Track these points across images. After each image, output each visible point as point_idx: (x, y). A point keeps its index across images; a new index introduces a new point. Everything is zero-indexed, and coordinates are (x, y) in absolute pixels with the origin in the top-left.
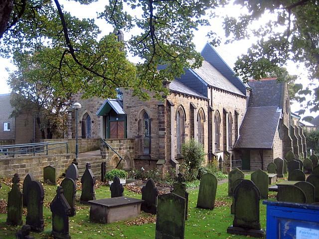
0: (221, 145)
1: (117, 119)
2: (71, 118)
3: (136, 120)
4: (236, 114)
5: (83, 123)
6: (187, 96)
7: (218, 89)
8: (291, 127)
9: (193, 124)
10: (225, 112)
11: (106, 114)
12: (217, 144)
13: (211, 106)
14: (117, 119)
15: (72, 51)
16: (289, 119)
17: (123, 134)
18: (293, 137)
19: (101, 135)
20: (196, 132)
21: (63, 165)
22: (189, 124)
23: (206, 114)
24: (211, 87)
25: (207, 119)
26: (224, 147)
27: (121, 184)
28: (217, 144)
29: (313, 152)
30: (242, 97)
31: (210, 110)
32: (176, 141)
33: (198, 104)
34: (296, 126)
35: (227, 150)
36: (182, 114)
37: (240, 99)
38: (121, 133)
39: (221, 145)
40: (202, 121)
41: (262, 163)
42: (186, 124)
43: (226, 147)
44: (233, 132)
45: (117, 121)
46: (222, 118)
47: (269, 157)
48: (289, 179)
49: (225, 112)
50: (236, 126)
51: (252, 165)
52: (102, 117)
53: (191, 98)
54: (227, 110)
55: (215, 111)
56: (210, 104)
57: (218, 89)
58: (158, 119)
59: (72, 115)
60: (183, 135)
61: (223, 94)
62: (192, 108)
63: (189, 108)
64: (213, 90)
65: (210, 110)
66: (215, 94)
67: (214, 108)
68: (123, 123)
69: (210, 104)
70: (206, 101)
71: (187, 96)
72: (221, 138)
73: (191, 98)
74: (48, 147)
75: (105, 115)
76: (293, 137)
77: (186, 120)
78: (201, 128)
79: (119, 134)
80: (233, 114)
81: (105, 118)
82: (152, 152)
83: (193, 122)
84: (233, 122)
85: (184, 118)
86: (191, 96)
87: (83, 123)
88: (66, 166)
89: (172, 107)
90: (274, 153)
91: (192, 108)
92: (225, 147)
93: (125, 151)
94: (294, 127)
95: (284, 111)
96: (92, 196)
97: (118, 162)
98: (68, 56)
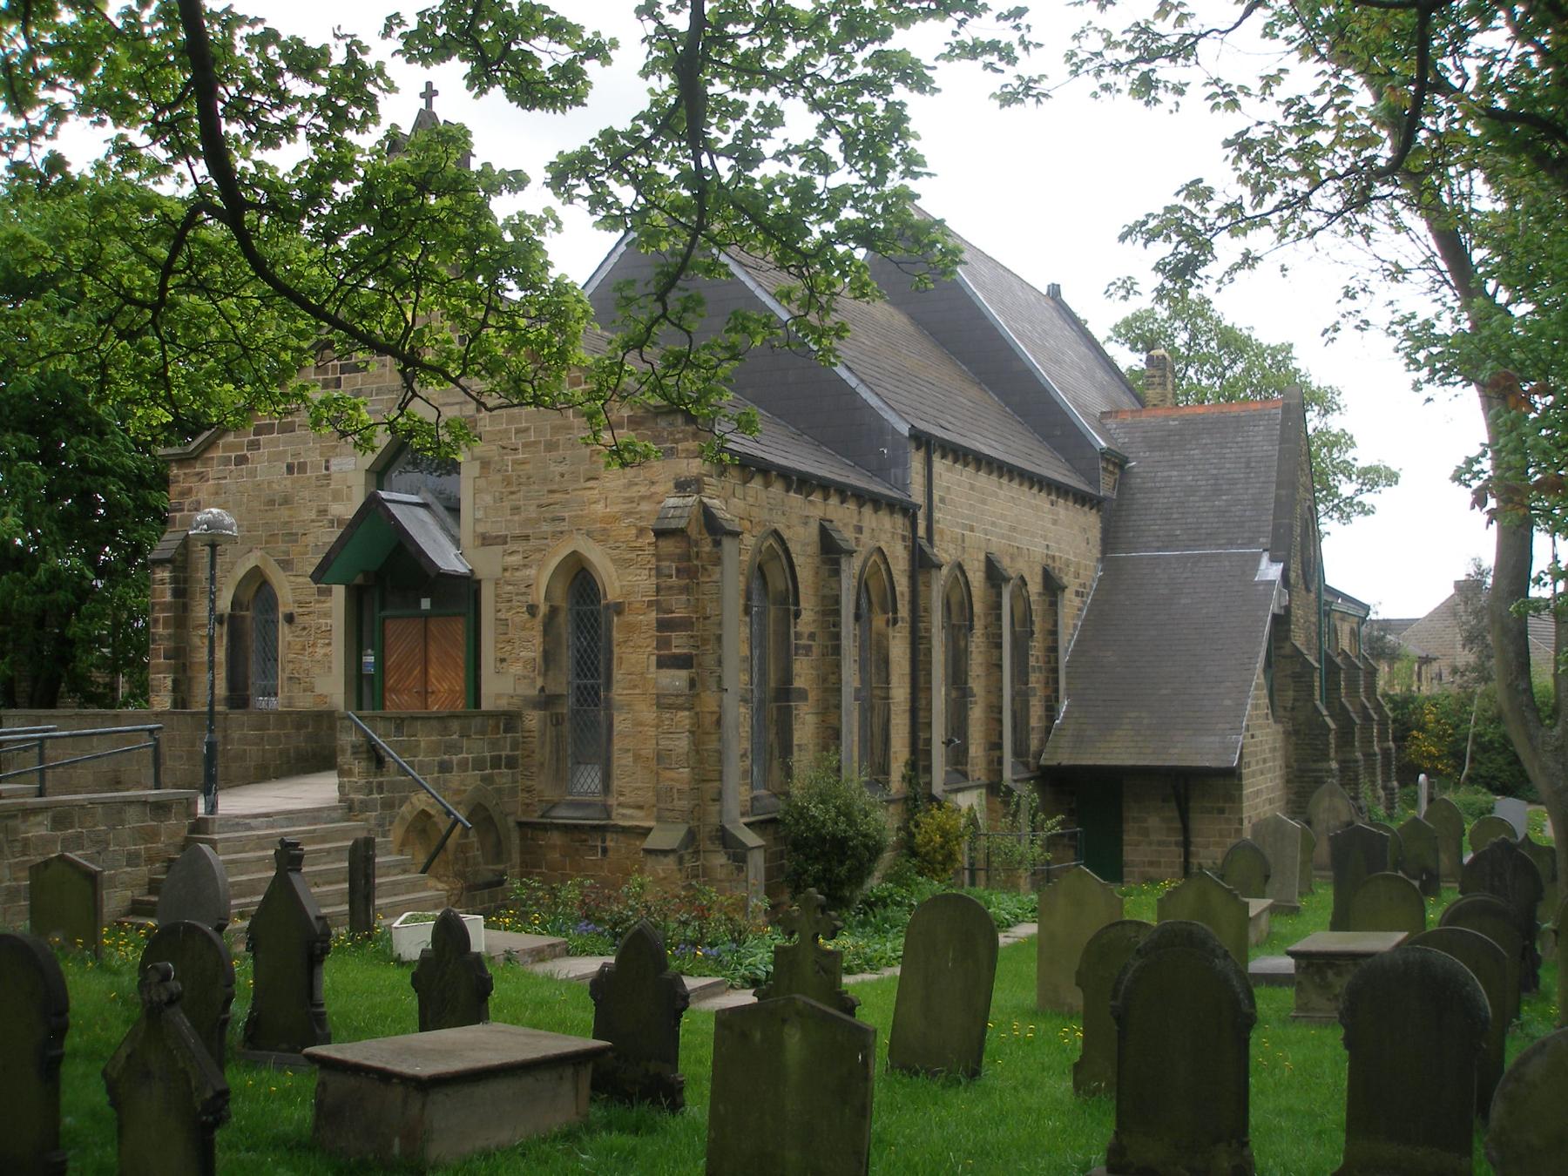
0: (976, 750)
1: (426, 604)
2: (168, 598)
3: (532, 610)
4: (1052, 586)
5: (234, 624)
6: (802, 483)
7: (960, 455)
8: (1331, 669)
9: (837, 637)
10: (994, 574)
11: (366, 573)
12: (958, 756)
13: (924, 542)
14: (426, 604)
15: (233, 212)
16: (1313, 619)
17: (459, 686)
18: (1341, 714)
19: (332, 688)
20: (850, 676)
21: (137, 855)
22: (812, 636)
23: (902, 585)
24: (922, 440)
25: (904, 611)
26: (990, 762)
27: (478, 955)
28: (958, 756)
29: (1431, 786)
30: (1082, 499)
31: (921, 562)
32: (745, 730)
33: (859, 529)
34: (1347, 656)
35: (1008, 775)
36: (778, 582)
37: (1066, 512)
38: (446, 686)
39: (976, 750)
40: (879, 621)
41: (1186, 844)
42: (798, 636)
43: (1000, 761)
44: (1036, 680)
45: (426, 616)
46: (978, 608)
47: (1221, 811)
48: (1340, 923)
49: (994, 574)
50: (1053, 649)
51: (1130, 854)
52: (339, 591)
53: (826, 499)
54: (1009, 567)
55: (945, 570)
56: (921, 531)
57: (960, 455)
58: (656, 605)
59: (175, 580)
60: (785, 693)
61: (984, 480)
62: (830, 549)
63: (813, 549)
64: (936, 458)
65: (921, 562)
66: (947, 475)
67: (944, 552)
68: (459, 627)
69: (921, 531)
70: (899, 519)
71: (802, 483)
72: (977, 713)
73: (826, 499)
74: (49, 752)
75: (359, 579)
76: (1341, 714)
77: (797, 615)
78: (876, 661)
79: (434, 684)
80: (1035, 587)
81: (357, 598)
82: (615, 784)
83: (837, 624)
84: (1037, 628)
85: (792, 598)
86: (826, 487)
87: (234, 624)
88: (150, 860)
89: (727, 543)
90: (1247, 791)
91: (830, 549)
92: (996, 765)
93: (472, 779)
94: (1338, 660)
95: (1293, 575)
96: (314, 1026)
97: (435, 843)
98: (214, 230)
